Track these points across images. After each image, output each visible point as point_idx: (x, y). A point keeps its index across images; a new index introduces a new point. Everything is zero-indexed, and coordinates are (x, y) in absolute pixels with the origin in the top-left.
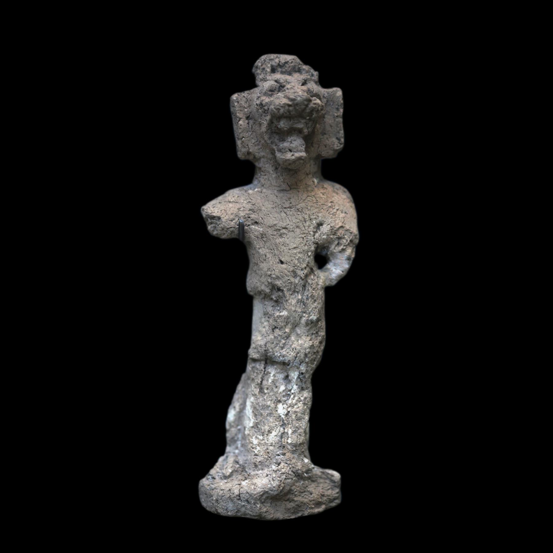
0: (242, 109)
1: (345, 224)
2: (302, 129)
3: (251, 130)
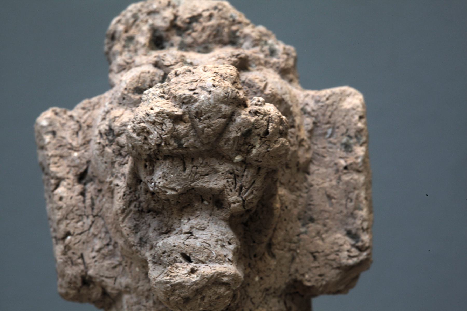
0: (64, 151)
2: (221, 191)
3: (89, 211)
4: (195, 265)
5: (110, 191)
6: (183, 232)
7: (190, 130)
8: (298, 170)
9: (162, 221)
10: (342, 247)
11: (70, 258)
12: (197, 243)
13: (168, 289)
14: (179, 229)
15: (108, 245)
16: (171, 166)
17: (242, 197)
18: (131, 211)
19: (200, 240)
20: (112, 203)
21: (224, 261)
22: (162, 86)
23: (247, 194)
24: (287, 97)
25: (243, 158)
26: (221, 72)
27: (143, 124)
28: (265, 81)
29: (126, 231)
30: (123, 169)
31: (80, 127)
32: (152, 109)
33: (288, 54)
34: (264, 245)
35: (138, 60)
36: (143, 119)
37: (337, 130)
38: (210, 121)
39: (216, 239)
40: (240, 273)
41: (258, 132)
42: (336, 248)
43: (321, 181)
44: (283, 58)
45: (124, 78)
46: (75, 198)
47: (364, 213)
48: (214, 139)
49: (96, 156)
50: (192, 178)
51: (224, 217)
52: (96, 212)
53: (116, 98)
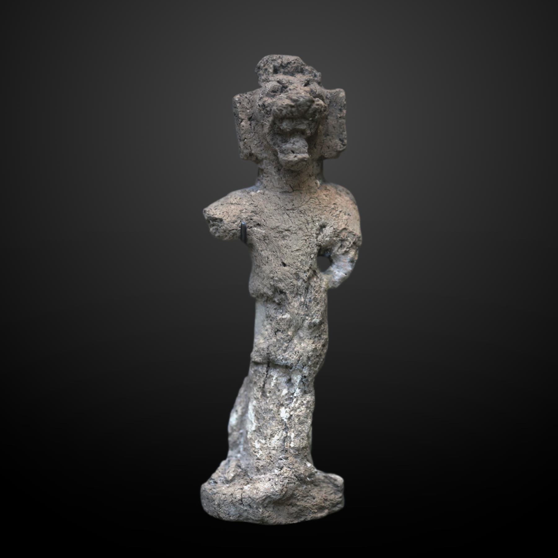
0: (244, 110)
1: (348, 226)
2: (305, 130)
3: (253, 131)
47: (345, 133)
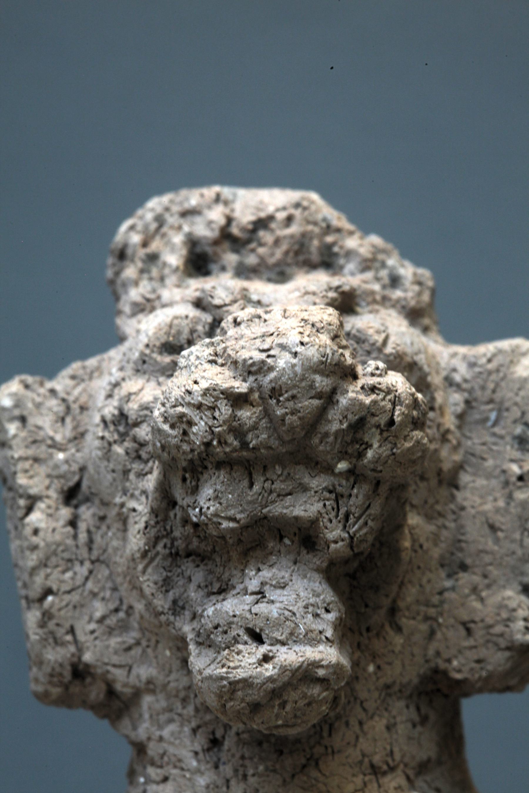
0: (41, 451)
2: (314, 522)
3: (84, 553)
4: (269, 648)
5: (120, 519)
6: (249, 591)
7: (260, 420)
8: (440, 482)
9: (211, 572)
10: (514, 614)
11: (52, 633)
12: (274, 611)
13: (223, 690)
14: (241, 586)
15: (117, 610)
16: (228, 480)
17: (348, 533)
18: (158, 554)
19: (278, 605)
20: (125, 539)
21: (319, 642)
22: (212, 344)
23: (356, 526)
24: (421, 359)
25: (350, 466)
26: (313, 319)
27: (180, 409)
28: (384, 331)
29: (148, 588)
30: (145, 482)
31: (68, 409)
32: (196, 382)
33: (420, 283)
34: (383, 612)
35: (166, 294)
36: (180, 400)
37: (505, 414)
38: (295, 403)
39: (304, 603)
40: (345, 662)
41: (378, 421)
42: (504, 615)
43: (478, 501)
44: (413, 291)
45: (143, 327)
46: (60, 530)
48: (303, 433)
49: (97, 460)
50: (265, 499)
51: (318, 566)
52: (95, 554)
53: (131, 362)
